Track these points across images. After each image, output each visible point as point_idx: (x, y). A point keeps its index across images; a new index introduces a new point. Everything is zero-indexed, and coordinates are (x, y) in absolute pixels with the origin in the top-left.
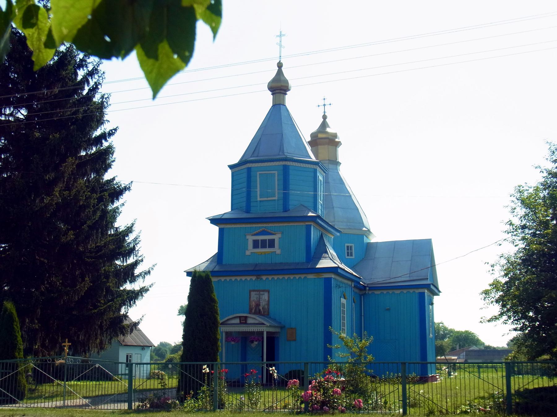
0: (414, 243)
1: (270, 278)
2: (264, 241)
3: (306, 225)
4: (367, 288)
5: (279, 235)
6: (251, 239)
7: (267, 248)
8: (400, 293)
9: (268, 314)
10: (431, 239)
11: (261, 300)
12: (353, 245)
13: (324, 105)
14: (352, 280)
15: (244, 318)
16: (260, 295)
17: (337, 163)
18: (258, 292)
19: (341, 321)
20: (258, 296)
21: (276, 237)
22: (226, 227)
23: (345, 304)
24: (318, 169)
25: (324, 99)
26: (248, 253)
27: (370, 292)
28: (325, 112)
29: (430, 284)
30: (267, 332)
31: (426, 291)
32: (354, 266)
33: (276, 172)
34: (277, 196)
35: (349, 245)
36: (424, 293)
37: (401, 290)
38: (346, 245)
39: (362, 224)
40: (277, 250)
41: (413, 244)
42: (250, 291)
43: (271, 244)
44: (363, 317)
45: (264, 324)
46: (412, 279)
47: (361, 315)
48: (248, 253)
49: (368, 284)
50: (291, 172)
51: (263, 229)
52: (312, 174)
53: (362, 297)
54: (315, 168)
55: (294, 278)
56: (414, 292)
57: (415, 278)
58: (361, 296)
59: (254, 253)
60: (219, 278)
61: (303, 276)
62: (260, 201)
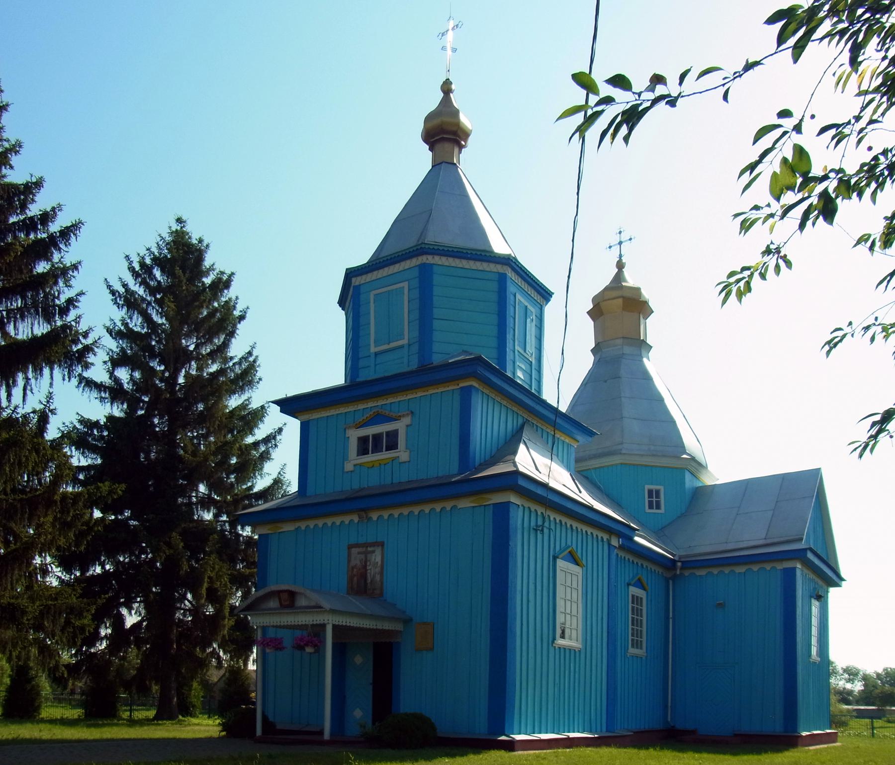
0: (785, 480)
1: (386, 514)
2: (377, 438)
3: (462, 388)
4: (679, 564)
5: (407, 420)
6: (354, 435)
7: (384, 453)
8: (745, 572)
9: (381, 594)
10: (819, 469)
11: (368, 563)
12: (661, 488)
13: (620, 243)
14: (610, 531)
15: (285, 596)
16: (366, 553)
17: (642, 346)
18: (363, 547)
19: (628, 626)
20: (363, 556)
21: (400, 426)
22: (313, 418)
23: (641, 599)
24: (510, 274)
25: (620, 233)
26: (349, 467)
27: (687, 573)
28: (621, 256)
29: (805, 550)
30: (335, 627)
31: (799, 566)
32: (662, 528)
33: (405, 285)
34: (406, 337)
35: (654, 487)
36: (794, 569)
37: (747, 567)
38: (647, 487)
39: (680, 447)
40: (402, 453)
41: (783, 479)
42: (350, 547)
43: (392, 441)
44: (671, 621)
45: (320, 607)
46: (769, 541)
47: (667, 618)
48: (349, 467)
49: (680, 557)
50: (437, 279)
51: (375, 410)
52: (494, 286)
53: (671, 582)
54: (501, 271)
55: (432, 509)
56: (773, 568)
57: (776, 540)
58: (667, 580)
59: (361, 465)
60: (298, 524)
61: (448, 505)
62: (376, 354)
